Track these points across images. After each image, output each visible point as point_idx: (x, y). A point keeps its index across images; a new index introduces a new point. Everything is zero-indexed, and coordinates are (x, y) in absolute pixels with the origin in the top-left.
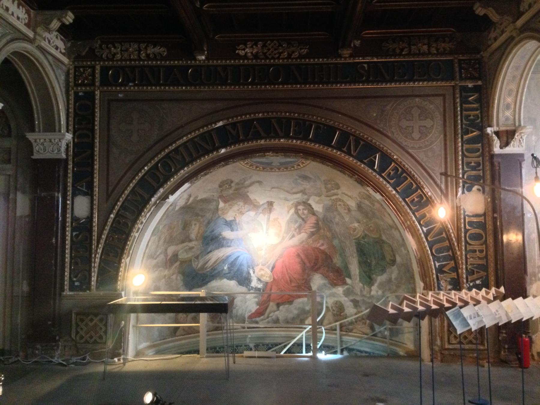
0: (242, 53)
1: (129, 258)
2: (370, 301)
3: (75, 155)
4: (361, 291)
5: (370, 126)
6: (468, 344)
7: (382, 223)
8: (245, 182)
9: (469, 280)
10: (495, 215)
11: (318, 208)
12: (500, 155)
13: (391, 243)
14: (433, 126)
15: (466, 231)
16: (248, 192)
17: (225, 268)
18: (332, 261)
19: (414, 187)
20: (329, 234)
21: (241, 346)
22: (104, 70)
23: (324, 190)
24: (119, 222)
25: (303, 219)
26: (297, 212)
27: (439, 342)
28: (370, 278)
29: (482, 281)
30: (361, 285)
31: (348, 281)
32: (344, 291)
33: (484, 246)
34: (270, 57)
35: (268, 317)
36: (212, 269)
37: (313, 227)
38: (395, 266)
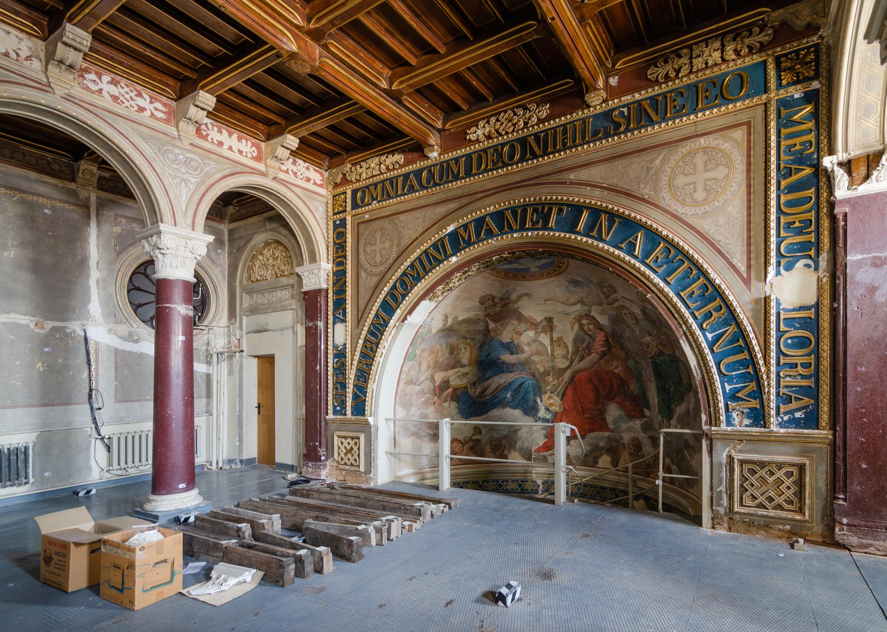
0: (473, 137)
3: (334, 284)
5: (628, 194)
6: (775, 508)
8: (509, 296)
9: (782, 410)
11: (603, 320)
12: (848, 201)
14: (727, 176)
15: (780, 334)
17: (508, 396)
18: (629, 388)
20: (621, 353)
22: (355, 192)
23: (602, 296)
24: (366, 347)
25: (590, 336)
26: (581, 327)
27: (725, 501)
30: (660, 417)
31: (646, 412)
32: (642, 425)
34: (503, 133)
37: (604, 346)
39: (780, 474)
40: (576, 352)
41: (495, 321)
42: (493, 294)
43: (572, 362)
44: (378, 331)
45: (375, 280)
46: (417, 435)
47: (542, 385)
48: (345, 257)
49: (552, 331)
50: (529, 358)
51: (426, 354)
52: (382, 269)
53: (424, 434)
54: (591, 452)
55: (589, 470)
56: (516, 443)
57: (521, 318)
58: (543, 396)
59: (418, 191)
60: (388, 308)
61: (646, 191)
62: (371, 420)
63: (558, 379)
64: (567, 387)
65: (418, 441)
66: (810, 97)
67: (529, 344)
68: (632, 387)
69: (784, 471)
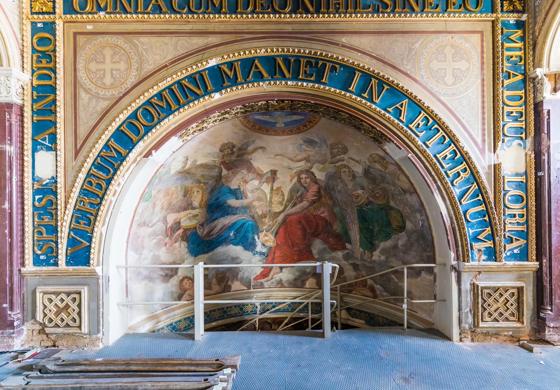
1: (106, 226)
2: (371, 265)
4: (361, 256)
7: (393, 188)
8: (247, 147)
9: (507, 249)
10: (540, 174)
11: (320, 176)
13: (401, 209)
14: (468, 68)
16: (251, 159)
17: (231, 234)
18: (332, 228)
19: (446, 141)
21: (247, 305)
23: (329, 156)
24: (90, 183)
25: (305, 188)
26: (299, 180)
28: (371, 243)
29: (520, 250)
30: (361, 249)
31: (348, 246)
32: (343, 255)
33: (525, 209)
35: (272, 278)
36: (218, 235)
37: (315, 196)
38: (404, 233)
39: (506, 295)
40: (289, 201)
41: (228, 169)
42: (235, 143)
43: (286, 207)
44: (108, 166)
45: (104, 105)
46: (149, 278)
47: (260, 225)
48: (54, 70)
49: (274, 182)
50: (251, 203)
51: (161, 195)
52: (117, 93)
53: (156, 276)
54: (300, 277)
55: (300, 291)
56: (238, 274)
57: (250, 168)
58: (260, 234)
59: (165, 13)
60: (125, 139)
61: (409, 67)
62: (98, 270)
63: (273, 221)
64: (280, 227)
65: (151, 284)
66: (520, 25)
67: (252, 192)
68: (335, 227)
69: (509, 292)
